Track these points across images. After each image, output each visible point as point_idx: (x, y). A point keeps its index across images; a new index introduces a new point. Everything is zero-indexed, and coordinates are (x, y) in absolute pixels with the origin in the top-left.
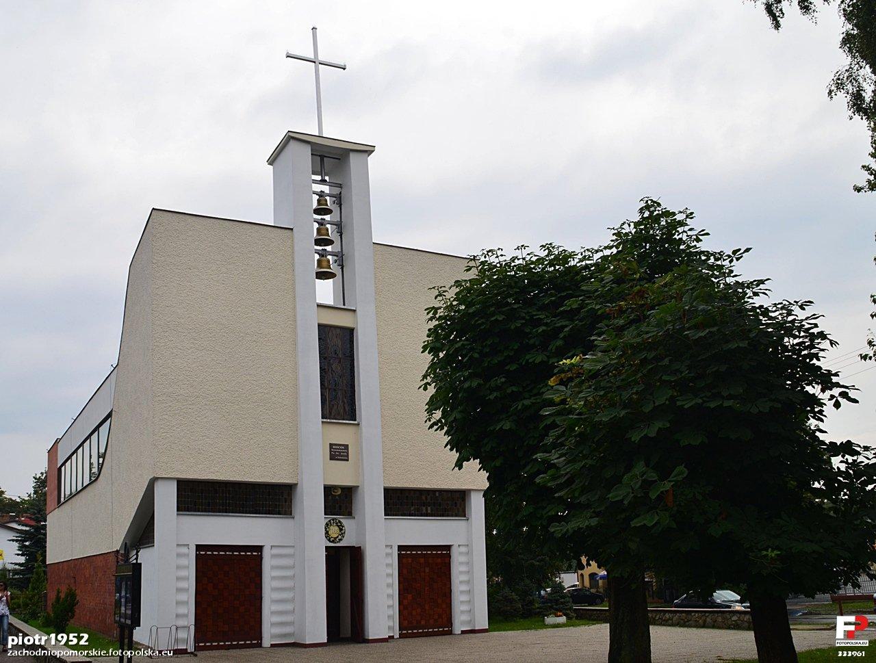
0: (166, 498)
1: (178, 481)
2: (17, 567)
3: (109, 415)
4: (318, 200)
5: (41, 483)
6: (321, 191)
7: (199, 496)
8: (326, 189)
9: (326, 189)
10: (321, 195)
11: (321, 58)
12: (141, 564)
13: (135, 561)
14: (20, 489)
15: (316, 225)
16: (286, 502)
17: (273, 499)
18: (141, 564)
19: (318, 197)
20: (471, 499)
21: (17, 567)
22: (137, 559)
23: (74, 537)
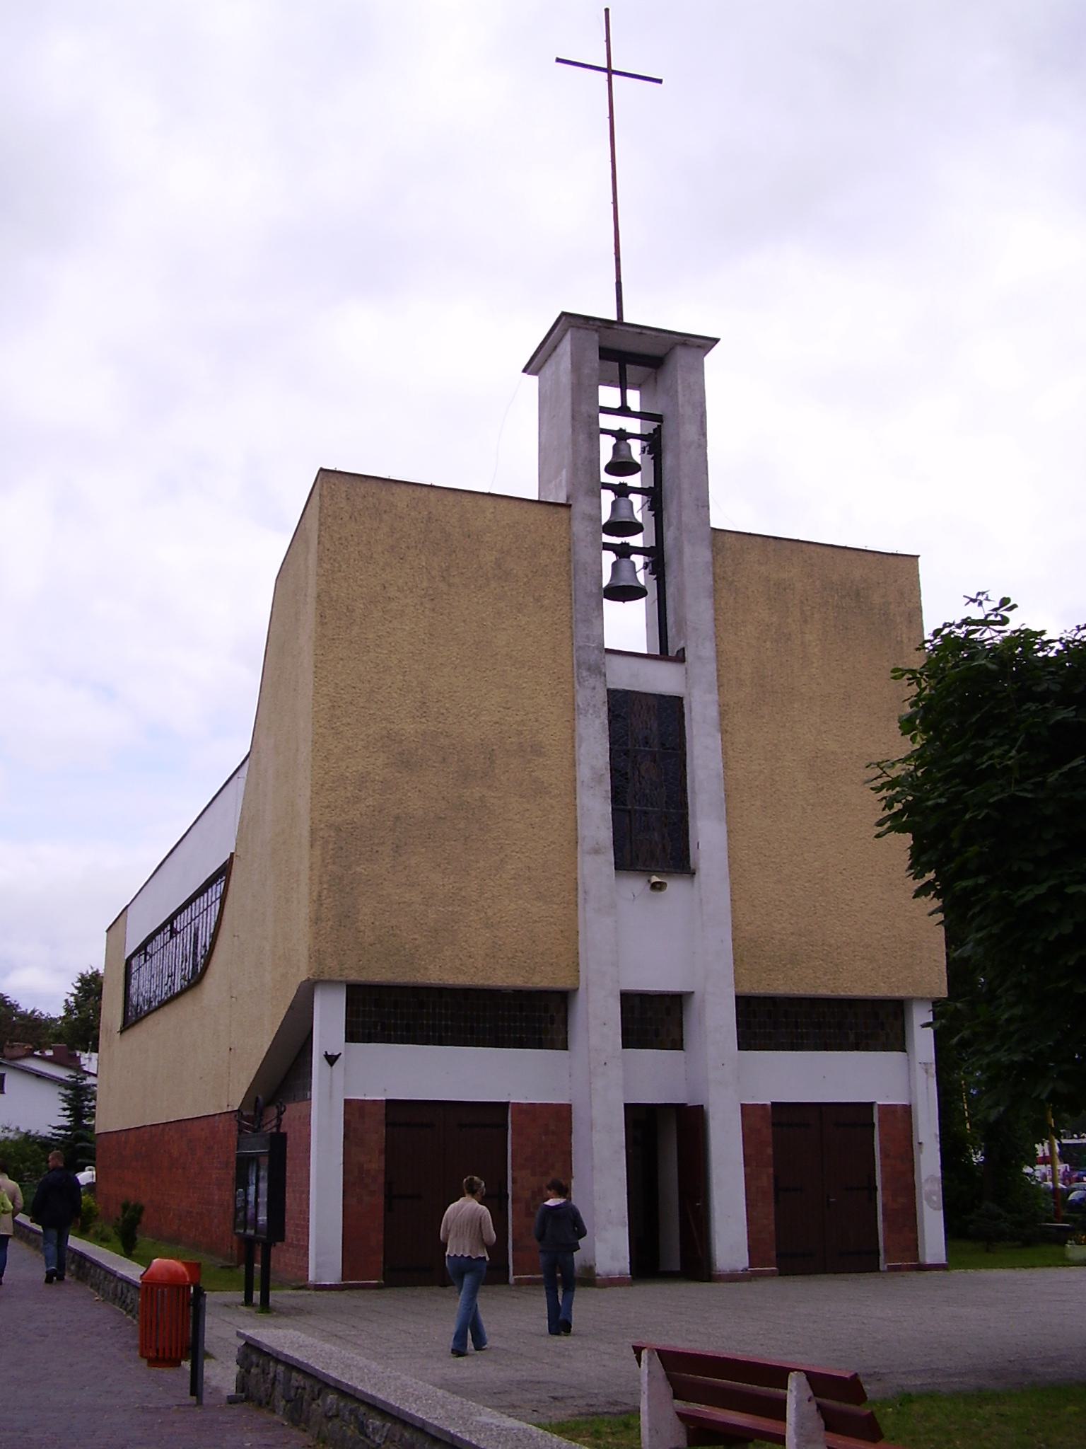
0: (329, 1018)
1: (348, 986)
2: (63, 1132)
3: (224, 872)
4: (615, 447)
5: (90, 987)
6: (621, 430)
7: (387, 1012)
8: (633, 425)
9: (633, 425)
10: (621, 436)
11: (613, 68)
12: (285, 1134)
13: (274, 1130)
14: (45, 991)
15: (609, 558)
16: (552, 1023)
17: (533, 1017)
18: (285, 1134)
19: (613, 441)
20: (309, 1087)
21: (63, 1132)
22: (278, 1126)
23: (142, 1084)
